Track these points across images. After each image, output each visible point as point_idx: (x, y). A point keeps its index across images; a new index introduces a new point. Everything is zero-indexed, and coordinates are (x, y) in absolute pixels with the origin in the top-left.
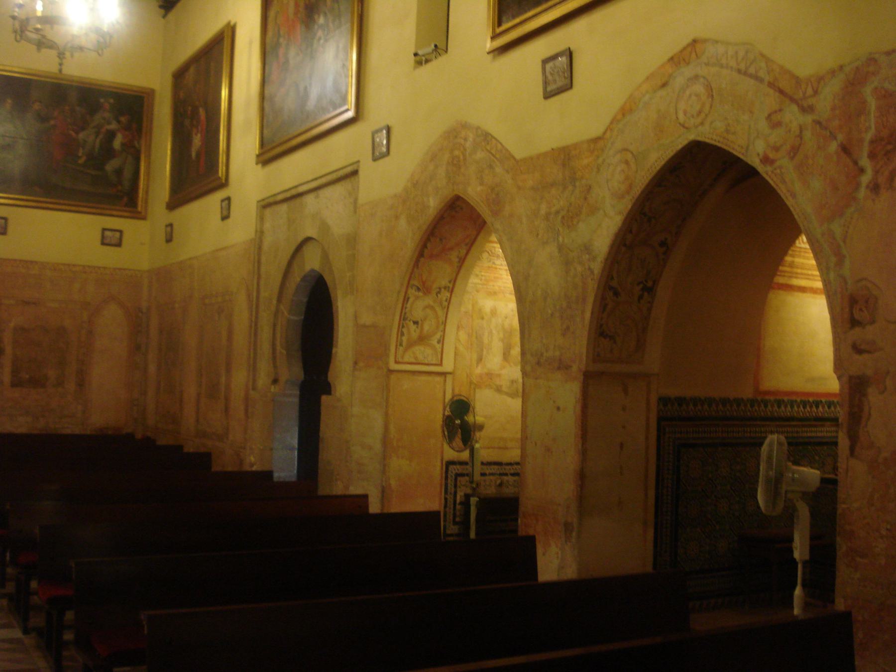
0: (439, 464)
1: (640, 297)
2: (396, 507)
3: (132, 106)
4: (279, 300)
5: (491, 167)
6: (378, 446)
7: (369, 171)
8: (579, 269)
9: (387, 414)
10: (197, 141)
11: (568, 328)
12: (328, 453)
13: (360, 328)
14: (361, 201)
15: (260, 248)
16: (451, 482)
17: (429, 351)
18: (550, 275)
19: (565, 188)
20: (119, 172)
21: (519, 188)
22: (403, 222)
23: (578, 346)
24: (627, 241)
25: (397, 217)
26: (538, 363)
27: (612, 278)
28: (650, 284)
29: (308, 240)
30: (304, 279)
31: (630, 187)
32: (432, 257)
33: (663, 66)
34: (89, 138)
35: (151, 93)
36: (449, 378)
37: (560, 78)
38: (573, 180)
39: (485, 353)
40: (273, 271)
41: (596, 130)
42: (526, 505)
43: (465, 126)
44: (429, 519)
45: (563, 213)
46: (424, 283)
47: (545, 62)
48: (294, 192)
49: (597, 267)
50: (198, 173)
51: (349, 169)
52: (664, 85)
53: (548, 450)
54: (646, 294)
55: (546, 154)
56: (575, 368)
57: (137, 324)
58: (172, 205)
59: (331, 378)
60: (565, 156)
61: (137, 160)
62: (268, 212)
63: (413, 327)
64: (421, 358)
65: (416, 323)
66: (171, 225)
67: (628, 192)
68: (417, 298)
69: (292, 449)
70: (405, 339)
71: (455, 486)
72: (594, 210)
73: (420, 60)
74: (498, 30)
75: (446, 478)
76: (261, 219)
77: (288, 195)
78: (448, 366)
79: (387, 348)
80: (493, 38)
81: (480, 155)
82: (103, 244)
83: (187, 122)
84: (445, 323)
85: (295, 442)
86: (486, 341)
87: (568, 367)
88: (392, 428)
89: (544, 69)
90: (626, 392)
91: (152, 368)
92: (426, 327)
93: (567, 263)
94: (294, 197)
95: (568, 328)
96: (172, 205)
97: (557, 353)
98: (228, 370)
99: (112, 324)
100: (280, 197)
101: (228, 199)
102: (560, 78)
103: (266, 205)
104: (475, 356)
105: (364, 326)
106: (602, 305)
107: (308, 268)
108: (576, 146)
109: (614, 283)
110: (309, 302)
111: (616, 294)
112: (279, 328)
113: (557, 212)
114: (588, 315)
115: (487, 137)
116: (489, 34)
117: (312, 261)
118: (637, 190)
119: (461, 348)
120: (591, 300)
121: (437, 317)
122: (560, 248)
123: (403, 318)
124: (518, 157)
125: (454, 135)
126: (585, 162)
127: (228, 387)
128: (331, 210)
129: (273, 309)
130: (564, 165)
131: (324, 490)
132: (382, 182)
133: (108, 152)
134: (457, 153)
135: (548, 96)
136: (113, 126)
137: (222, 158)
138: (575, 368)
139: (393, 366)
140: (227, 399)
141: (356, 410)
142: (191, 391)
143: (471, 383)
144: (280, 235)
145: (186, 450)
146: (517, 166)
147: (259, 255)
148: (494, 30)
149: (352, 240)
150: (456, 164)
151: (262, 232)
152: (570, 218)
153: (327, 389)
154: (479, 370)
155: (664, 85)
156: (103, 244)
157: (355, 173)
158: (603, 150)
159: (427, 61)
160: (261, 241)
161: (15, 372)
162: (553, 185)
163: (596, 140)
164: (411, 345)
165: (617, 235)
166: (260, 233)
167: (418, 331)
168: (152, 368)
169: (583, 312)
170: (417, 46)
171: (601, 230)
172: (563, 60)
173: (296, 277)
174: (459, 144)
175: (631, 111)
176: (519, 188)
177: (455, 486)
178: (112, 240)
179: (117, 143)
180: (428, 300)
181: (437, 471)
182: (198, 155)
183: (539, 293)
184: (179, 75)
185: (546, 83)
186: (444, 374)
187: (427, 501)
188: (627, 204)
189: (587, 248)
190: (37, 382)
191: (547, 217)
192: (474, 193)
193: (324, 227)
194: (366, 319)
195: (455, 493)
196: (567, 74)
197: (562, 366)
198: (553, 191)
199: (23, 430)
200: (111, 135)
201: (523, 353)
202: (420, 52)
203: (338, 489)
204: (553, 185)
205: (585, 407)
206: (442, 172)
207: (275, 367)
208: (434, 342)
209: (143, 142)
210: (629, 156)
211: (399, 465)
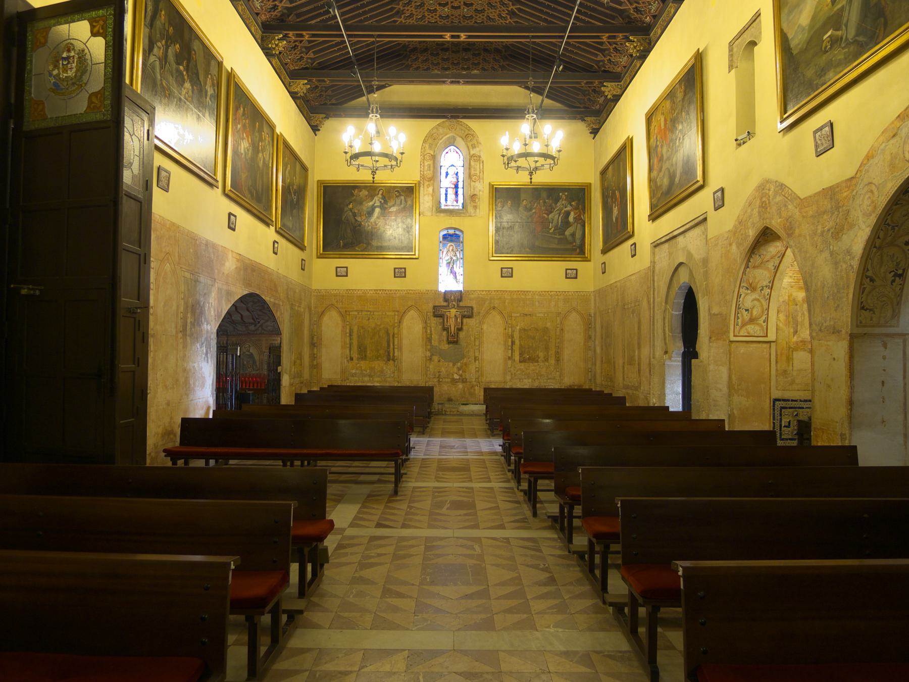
0: (768, 401)
1: (893, 281)
2: (738, 427)
3: (578, 195)
4: (666, 303)
5: (786, 206)
6: (725, 389)
7: (712, 215)
8: (844, 266)
9: (730, 369)
10: (615, 211)
11: (838, 306)
12: (696, 396)
13: (712, 316)
14: (709, 237)
15: (654, 272)
16: (777, 412)
17: (757, 328)
18: (825, 272)
19: (833, 214)
20: (573, 235)
21: (803, 217)
22: (734, 247)
23: (844, 316)
24: (874, 245)
25: (730, 245)
26: (820, 330)
27: (868, 270)
28: (900, 272)
29: (681, 264)
30: (680, 288)
31: (875, 207)
32: (754, 267)
33: (893, 123)
34: (555, 218)
35: (589, 185)
36: (773, 345)
37: (826, 141)
38: (838, 208)
39: (799, 327)
40: (662, 283)
41: (850, 173)
42: (816, 424)
43: (768, 181)
44: (767, 437)
45: (832, 231)
46: (751, 285)
47: (815, 132)
48: (671, 235)
49: (855, 263)
50: (618, 231)
51: (702, 218)
52: (894, 136)
53: (829, 386)
54: (897, 279)
55: (818, 193)
56: (844, 332)
57: (588, 325)
58: (605, 251)
59: (698, 348)
60: (831, 192)
61: (584, 226)
62: (657, 249)
63: (745, 313)
64: (752, 333)
65: (747, 310)
66: (604, 263)
67: (873, 212)
68: (747, 294)
69: (678, 394)
70: (740, 321)
71: (781, 415)
72: (852, 226)
73: (740, 143)
74: (785, 116)
75: (774, 409)
76: (654, 254)
77: (668, 237)
78: (772, 336)
79: (728, 327)
80: (781, 122)
81: (778, 199)
82: (337, 276)
83: (609, 200)
84: (768, 309)
85: (680, 390)
86: (800, 319)
87: (839, 332)
88: (734, 377)
89: (815, 138)
90: (885, 346)
91: (598, 350)
92: (755, 313)
93: (836, 263)
94: (671, 238)
95: (838, 306)
96: (605, 251)
97: (832, 323)
98: (639, 348)
99: (574, 326)
100: (663, 240)
101: (635, 244)
102: (826, 141)
103: (656, 245)
104: (792, 330)
105: (714, 314)
106: (861, 288)
107: (682, 281)
108: (838, 185)
109: (870, 274)
110: (685, 303)
111: (872, 280)
112: (667, 321)
113: (829, 230)
114: (851, 296)
115: (782, 186)
116: (779, 120)
117: (683, 277)
118: (879, 210)
119: (781, 325)
120: (852, 286)
121: (762, 305)
122: (831, 254)
123: (738, 307)
124: (802, 197)
125: (762, 188)
126: (845, 194)
127: (639, 358)
128: (693, 242)
129: (663, 308)
130: (831, 199)
131: (694, 417)
132: (722, 223)
133: (566, 224)
134: (764, 199)
135: (818, 155)
136: (569, 208)
137: (630, 220)
138: (844, 332)
139: (732, 338)
140: (639, 364)
141: (712, 367)
142: (620, 362)
143: (790, 348)
144: (665, 263)
145: (671, 409)
146: (803, 203)
147: (654, 276)
148: (781, 117)
149: (705, 261)
150: (764, 206)
151: (654, 262)
152: (838, 233)
153: (695, 355)
154: (795, 339)
155: (894, 136)
156: (337, 276)
157: (705, 219)
158: (856, 185)
159: (744, 143)
160: (654, 267)
161: (521, 354)
162: (824, 212)
163: (852, 178)
164: (744, 325)
165: (868, 241)
166: (653, 263)
167: (749, 315)
168: (598, 350)
169: (847, 294)
170: (738, 134)
171: (858, 239)
172: (827, 129)
173: (675, 287)
174: (769, 193)
175: (873, 157)
176: (803, 217)
177: (781, 415)
178: (572, 275)
179: (571, 219)
180: (755, 295)
181: (767, 405)
182: (617, 219)
183: (819, 284)
184: (603, 173)
185: (817, 146)
186: (770, 342)
187: (763, 425)
188: (873, 220)
189: (849, 252)
190: (533, 360)
191: (822, 234)
192: (776, 224)
193: (690, 255)
194: (715, 310)
195: (781, 420)
196: (830, 138)
197: (836, 331)
198: (825, 217)
199: (527, 387)
200: (568, 214)
201: (811, 324)
202: (739, 138)
203: (703, 416)
204: (824, 212)
205: (851, 357)
206: (756, 212)
207: (666, 344)
208: (761, 321)
209: (586, 215)
210: (873, 187)
211: (740, 401)
